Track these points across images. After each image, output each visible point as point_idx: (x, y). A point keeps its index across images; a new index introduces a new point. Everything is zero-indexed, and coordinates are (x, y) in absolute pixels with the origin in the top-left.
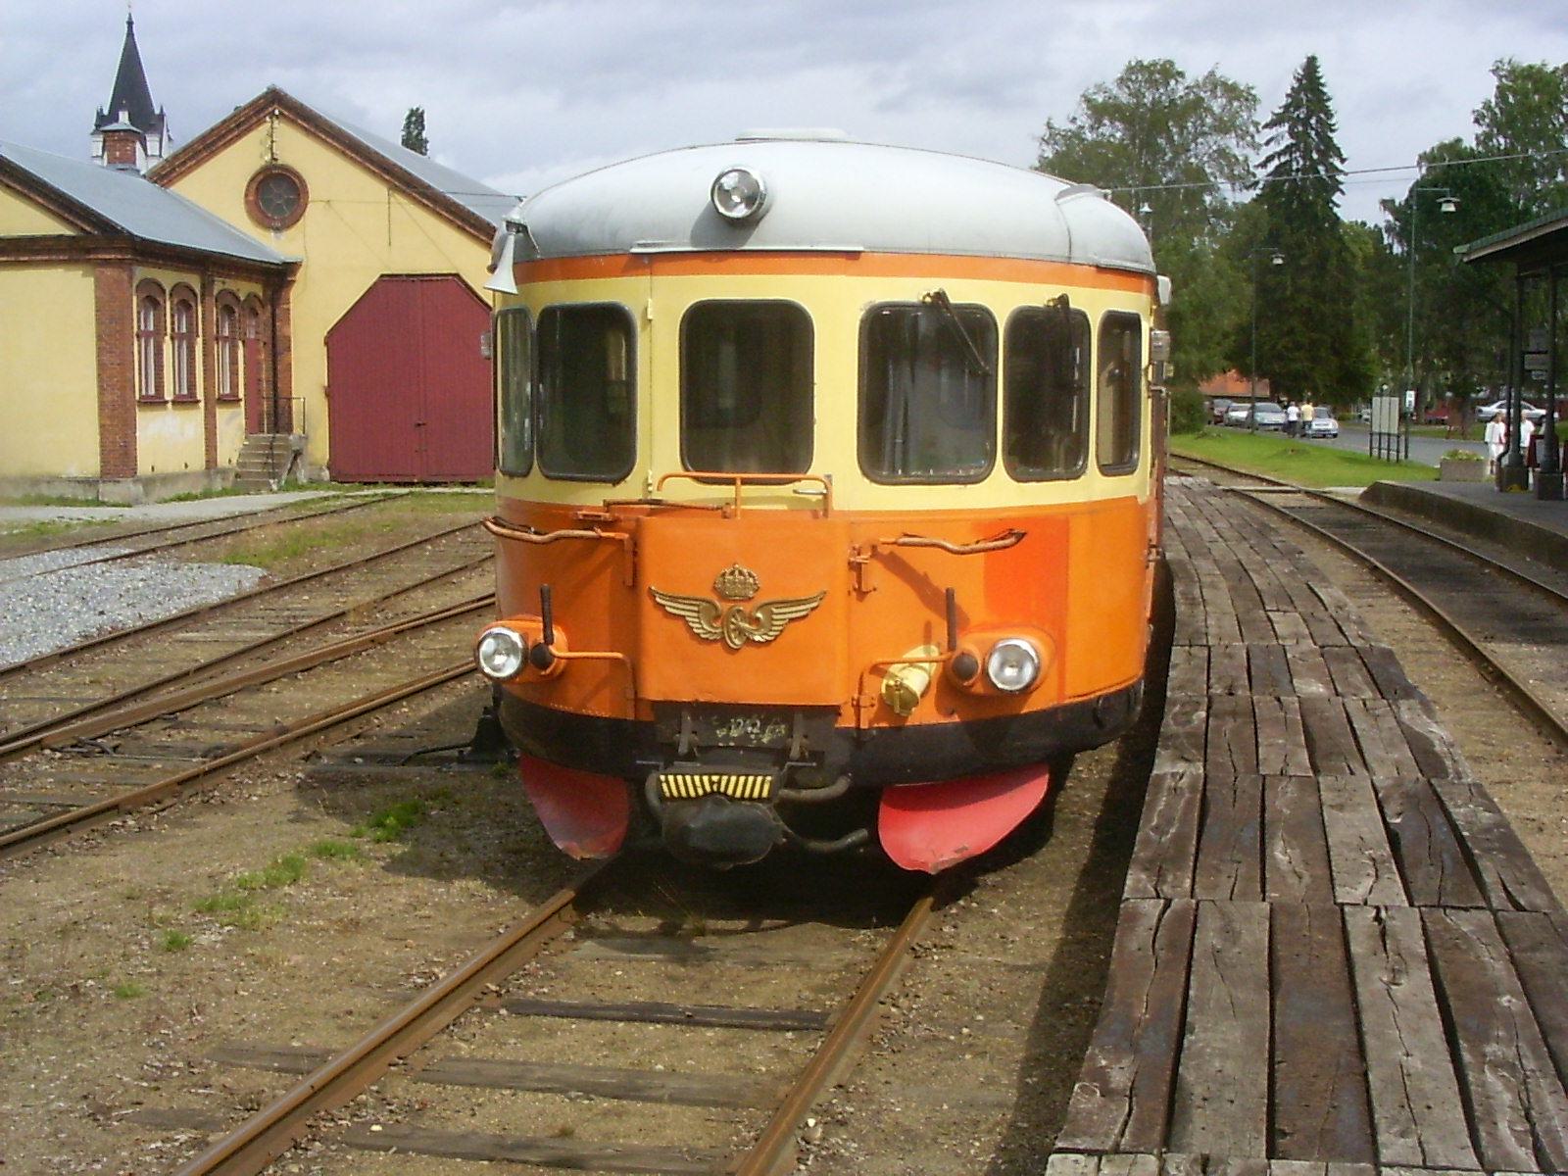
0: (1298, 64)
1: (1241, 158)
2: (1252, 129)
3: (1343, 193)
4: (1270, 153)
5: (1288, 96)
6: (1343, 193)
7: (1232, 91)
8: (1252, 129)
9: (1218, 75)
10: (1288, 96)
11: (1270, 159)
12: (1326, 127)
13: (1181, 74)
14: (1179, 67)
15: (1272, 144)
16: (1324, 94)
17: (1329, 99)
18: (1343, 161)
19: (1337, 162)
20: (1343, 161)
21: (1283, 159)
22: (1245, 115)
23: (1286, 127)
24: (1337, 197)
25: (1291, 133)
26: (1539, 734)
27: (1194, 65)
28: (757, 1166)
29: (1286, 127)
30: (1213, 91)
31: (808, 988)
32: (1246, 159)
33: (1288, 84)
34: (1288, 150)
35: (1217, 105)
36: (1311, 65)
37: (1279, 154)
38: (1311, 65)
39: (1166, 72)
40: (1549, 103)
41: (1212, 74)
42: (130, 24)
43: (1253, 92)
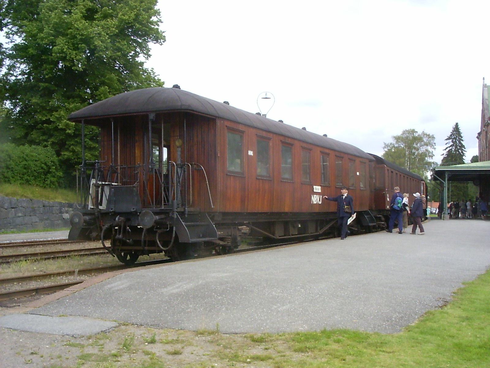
0: (453, 125)
1: (431, 152)
2: (434, 145)
3: (465, 156)
4: (447, 147)
5: (451, 133)
6: (465, 156)
7: (428, 136)
8: (434, 145)
9: (425, 132)
10: (451, 133)
11: (447, 148)
12: (461, 140)
13: (417, 132)
14: (416, 130)
15: (447, 144)
16: (460, 132)
17: (461, 133)
18: (465, 148)
19: (463, 149)
20: (465, 148)
21: (451, 148)
22: (432, 141)
23: (451, 140)
24: (464, 157)
25: (452, 141)
26: (10, 183)
27: (419, 131)
28: (251, 248)
29: (451, 140)
30: (424, 136)
31: (104, 46)
32: (432, 152)
33: (451, 130)
34: (451, 146)
35: (425, 140)
36: (457, 124)
37: (449, 147)
38: (457, 124)
39: (413, 131)
40: (61, 357)
41: (423, 132)
42: (262, 98)
43: (434, 136)
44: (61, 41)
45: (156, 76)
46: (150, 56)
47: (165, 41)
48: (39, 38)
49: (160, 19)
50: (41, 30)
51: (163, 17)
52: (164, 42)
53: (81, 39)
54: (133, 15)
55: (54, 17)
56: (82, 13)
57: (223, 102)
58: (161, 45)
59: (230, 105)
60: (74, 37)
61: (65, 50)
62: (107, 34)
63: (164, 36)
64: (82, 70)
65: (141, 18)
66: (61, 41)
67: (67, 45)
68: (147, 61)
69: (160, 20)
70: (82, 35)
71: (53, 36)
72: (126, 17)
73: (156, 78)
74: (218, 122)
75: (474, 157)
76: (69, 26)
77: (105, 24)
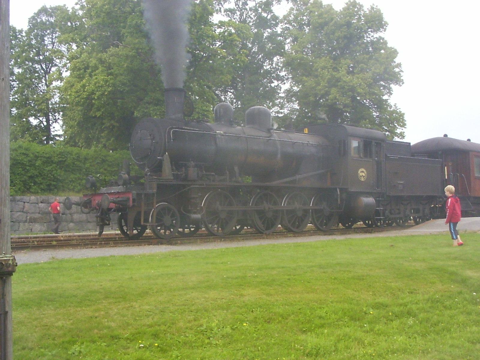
17: (405, 121)
44: (334, 90)
45: (398, 109)
46: (391, 94)
47: (403, 83)
48: (318, 90)
49: (402, 69)
50: (318, 84)
51: (403, 68)
52: (402, 84)
53: (348, 89)
54: (382, 69)
55: (327, 75)
56: (346, 70)
57: (443, 136)
58: (401, 86)
59: (471, 141)
60: (343, 88)
61: (337, 97)
62: (366, 84)
63: (403, 80)
64: (298, 102)
65: (388, 70)
66: (334, 90)
67: (338, 94)
68: (389, 98)
69: (402, 70)
70: (349, 86)
71: (327, 88)
72: (378, 71)
73: (398, 111)
74: (471, 153)
75: (402, 115)
76: (338, 80)
77: (363, 77)
